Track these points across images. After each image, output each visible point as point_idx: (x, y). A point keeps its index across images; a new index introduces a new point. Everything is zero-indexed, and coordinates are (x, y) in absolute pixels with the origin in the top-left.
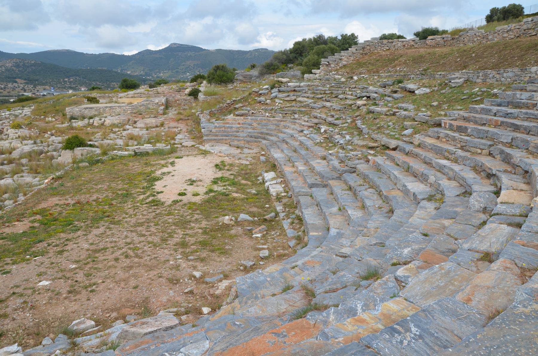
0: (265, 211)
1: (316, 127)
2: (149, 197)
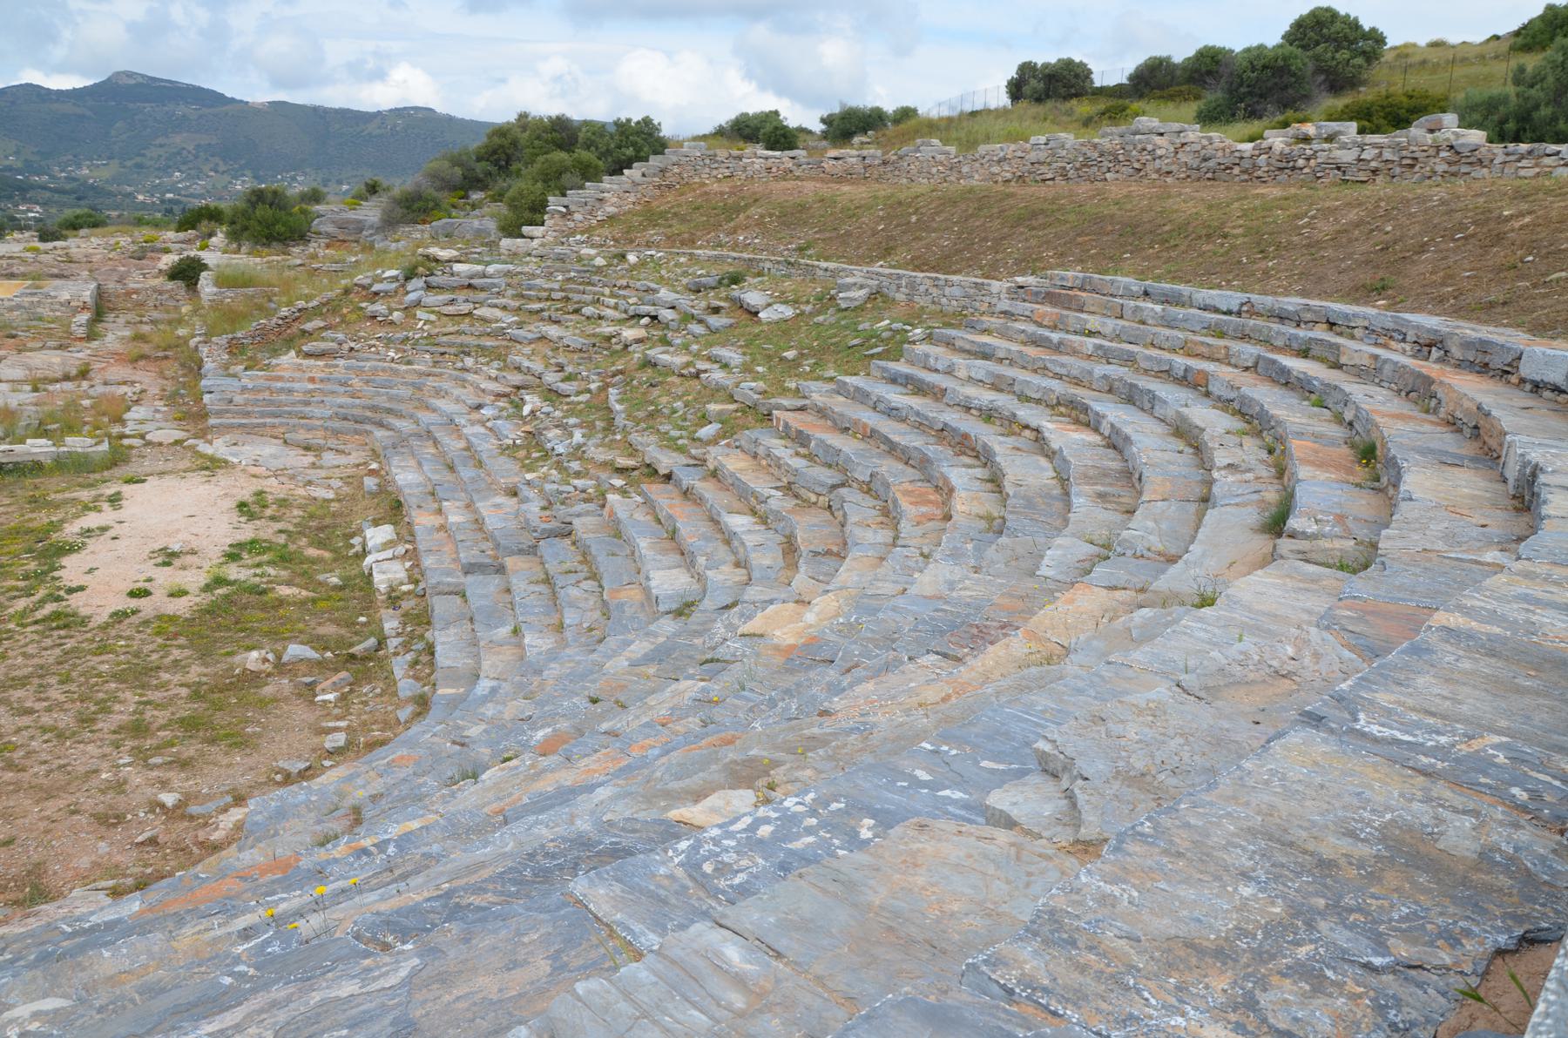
0: (356, 633)
1: (513, 397)
2: (42, 602)
